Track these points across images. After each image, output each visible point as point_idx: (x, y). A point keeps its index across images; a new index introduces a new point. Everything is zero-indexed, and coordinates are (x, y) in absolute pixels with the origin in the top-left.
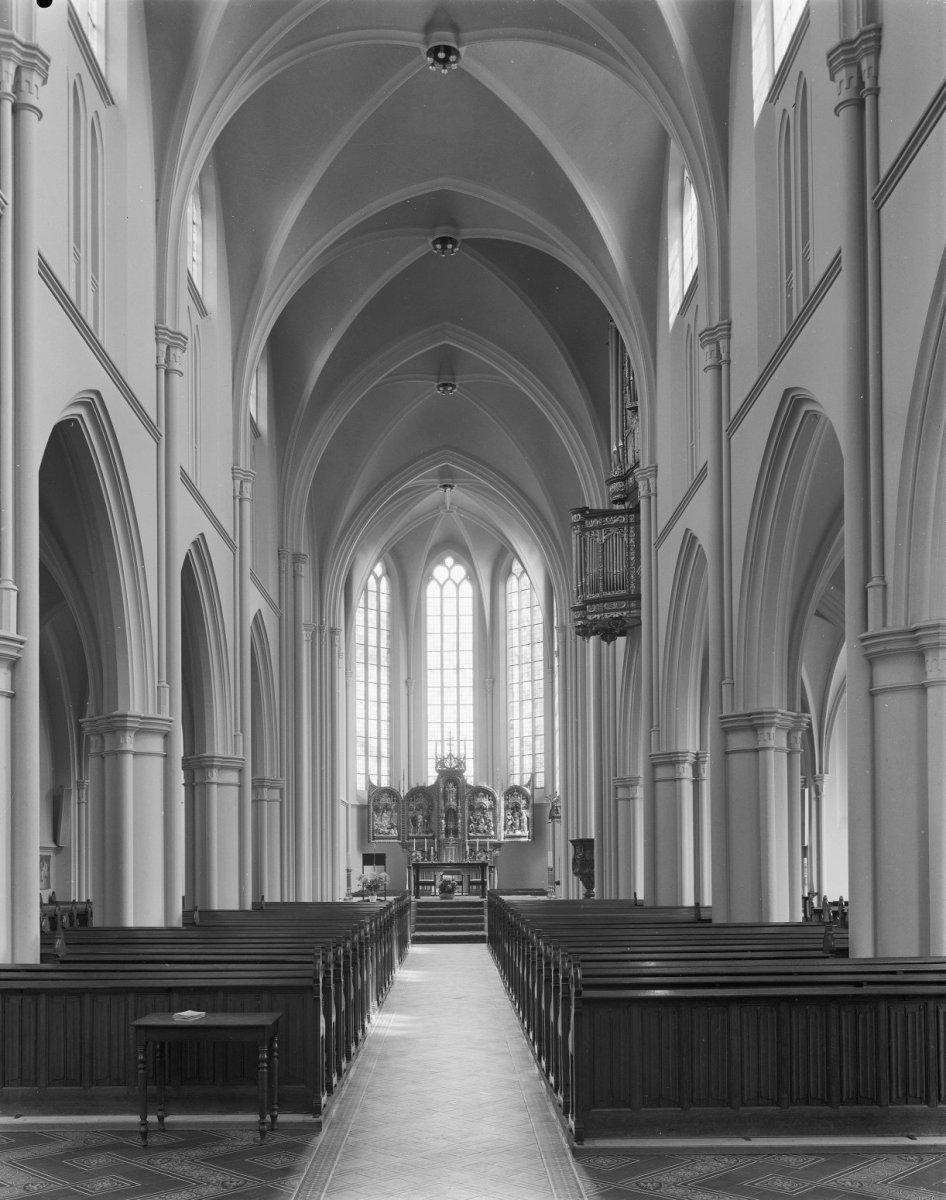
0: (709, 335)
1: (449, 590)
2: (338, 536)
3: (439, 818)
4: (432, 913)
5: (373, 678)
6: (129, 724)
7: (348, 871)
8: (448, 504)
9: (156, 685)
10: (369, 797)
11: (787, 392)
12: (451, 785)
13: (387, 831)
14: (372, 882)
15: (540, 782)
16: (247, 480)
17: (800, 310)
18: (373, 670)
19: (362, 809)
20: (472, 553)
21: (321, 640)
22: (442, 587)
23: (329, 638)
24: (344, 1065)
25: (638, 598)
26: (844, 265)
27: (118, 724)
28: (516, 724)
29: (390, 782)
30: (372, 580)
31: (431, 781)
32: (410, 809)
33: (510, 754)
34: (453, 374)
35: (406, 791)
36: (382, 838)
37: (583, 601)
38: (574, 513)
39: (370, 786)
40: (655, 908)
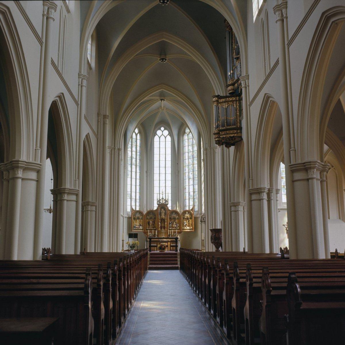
0: (242, 78)
1: (162, 141)
2: (121, 116)
3: (158, 222)
4: (156, 257)
5: (134, 170)
6: (20, 165)
7: (123, 241)
8: (162, 107)
9: (34, 148)
10: (132, 214)
11: (265, 94)
12: (163, 210)
13: (138, 227)
14: (132, 245)
15: (196, 208)
16: (84, 79)
17: (269, 72)
18: (134, 167)
19: (129, 218)
20: (171, 126)
21: (114, 153)
22: (160, 138)
23: (118, 153)
24: (117, 330)
25: (240, 128)
26: (280, 62)
27: (15, 165)
28: (187, 187)
29: (140, 208)
30: (134, 135)
31: (155, 208)
32: (147, 219)
33: (185, 198)
34: (166, 55)
35: (146, 212)
36: (137, 230)
37: (218, 130)
38: (214, 98)
39: (132, 209)
40: (253, 254)
